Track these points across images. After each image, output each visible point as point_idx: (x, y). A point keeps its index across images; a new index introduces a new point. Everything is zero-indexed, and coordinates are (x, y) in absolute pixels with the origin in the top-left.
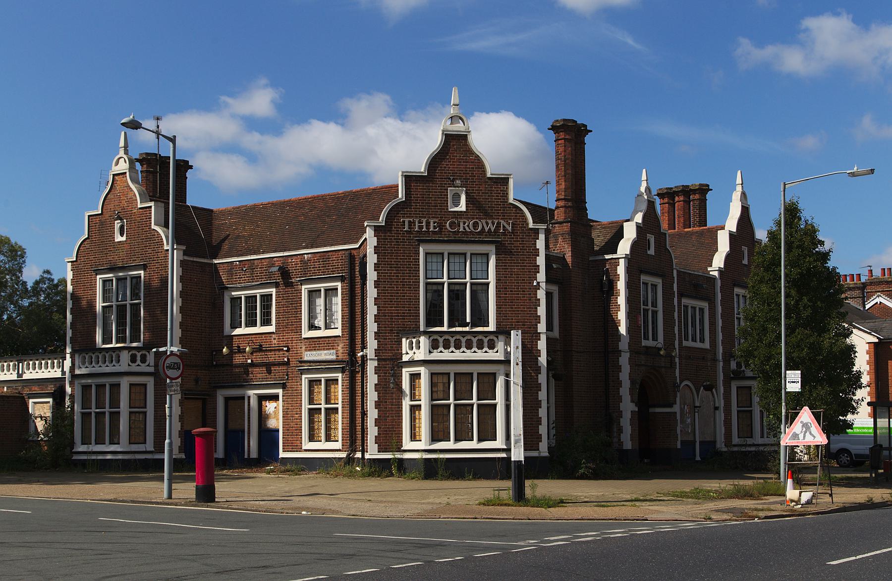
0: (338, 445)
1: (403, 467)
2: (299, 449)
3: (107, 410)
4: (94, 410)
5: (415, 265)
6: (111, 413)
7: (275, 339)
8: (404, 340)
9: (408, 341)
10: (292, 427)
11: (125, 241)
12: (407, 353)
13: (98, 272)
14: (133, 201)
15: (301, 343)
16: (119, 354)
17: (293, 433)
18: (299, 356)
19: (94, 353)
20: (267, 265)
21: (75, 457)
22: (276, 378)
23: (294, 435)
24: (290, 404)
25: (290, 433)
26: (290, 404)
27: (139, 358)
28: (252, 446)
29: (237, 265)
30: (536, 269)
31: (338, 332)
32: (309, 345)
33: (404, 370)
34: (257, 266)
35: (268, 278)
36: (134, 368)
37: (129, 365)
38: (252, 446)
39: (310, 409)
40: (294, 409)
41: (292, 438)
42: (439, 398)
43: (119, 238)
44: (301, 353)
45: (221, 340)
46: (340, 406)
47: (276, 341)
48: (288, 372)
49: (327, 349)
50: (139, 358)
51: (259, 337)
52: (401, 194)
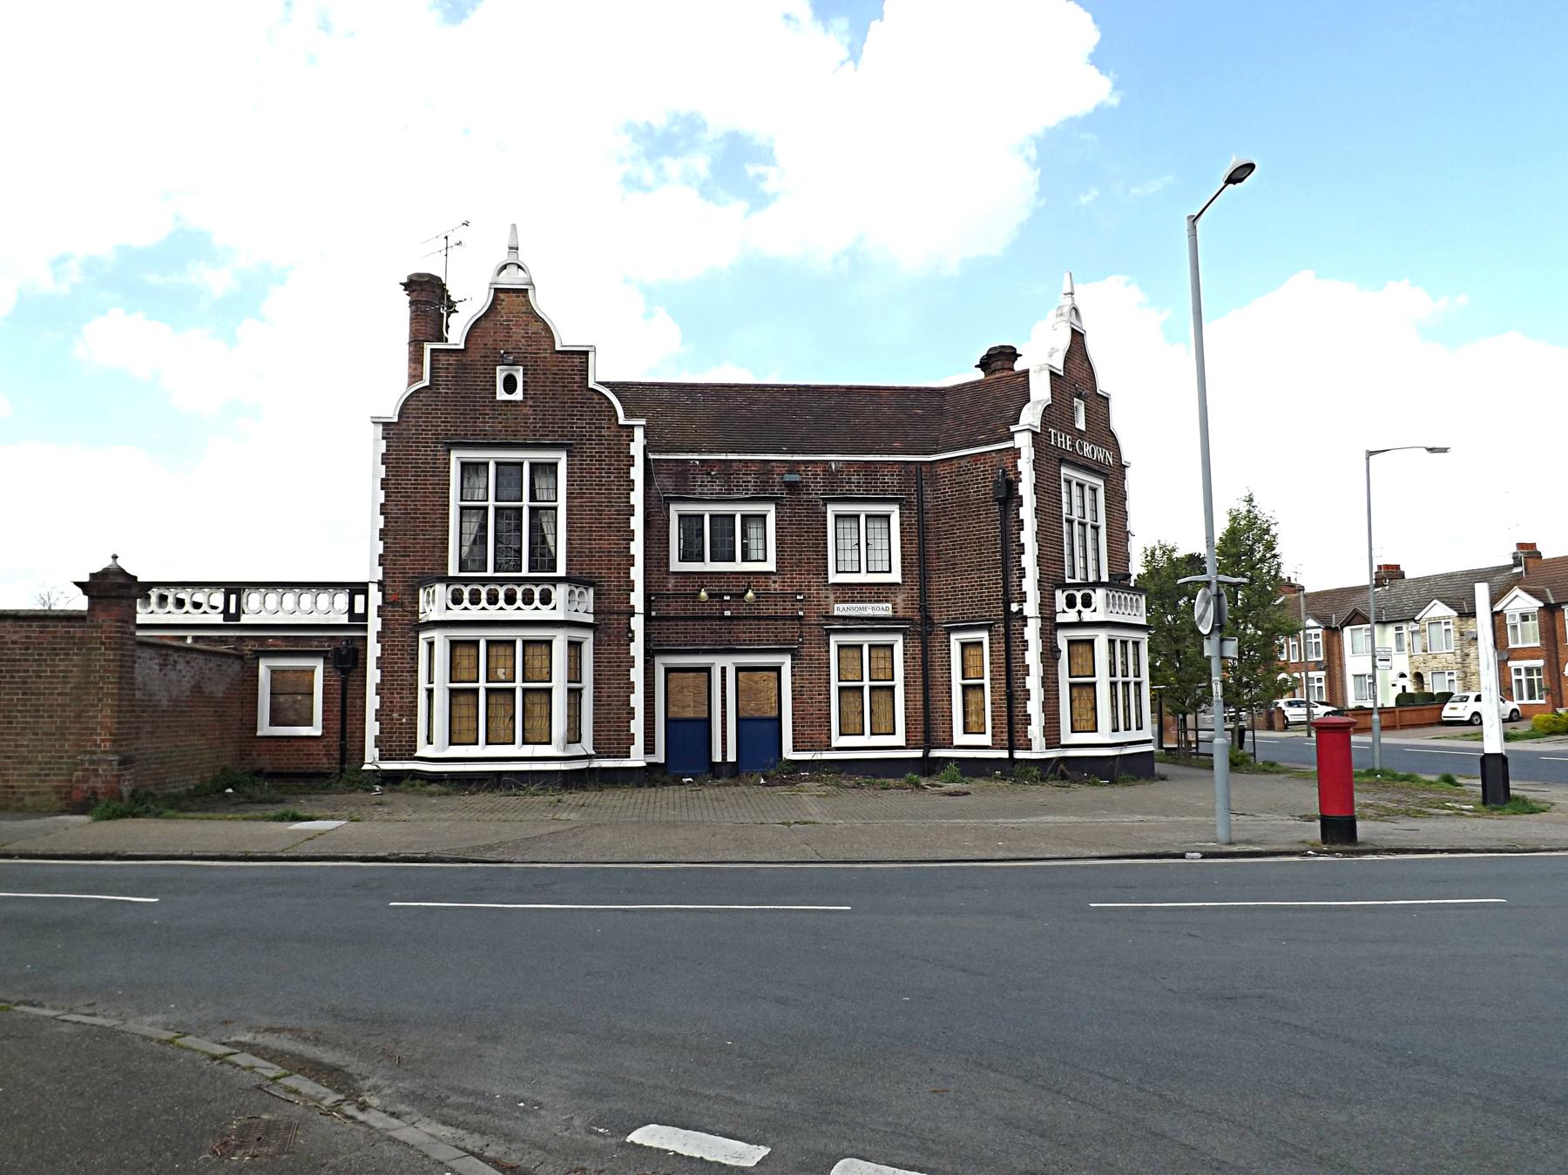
2: (829, 748)
7: (775, 582)
8: (421, 591)
11: (521, 402)
12: (1064, 612)
13: (450, 446)
14: (540, 337)
15: (828, 590)
16: (1090, 596)
19: (577, 587)
21: (732, 757)
22: (779, 640)
26: (807, 679)
27: (1079, 600)
28: (725, 746)
29: (697, 466)
30: (630, 510)
31: (896, 577)
35: (760, 490)
36: (457, 613)
37: (554, 608)
38: (725, 746)
42: (463, 679)
43: (501, 395)
45: (664, 578)
46: (987, 682)
47: (777, 585)
49: (876, 602)
50: (1079, 600)
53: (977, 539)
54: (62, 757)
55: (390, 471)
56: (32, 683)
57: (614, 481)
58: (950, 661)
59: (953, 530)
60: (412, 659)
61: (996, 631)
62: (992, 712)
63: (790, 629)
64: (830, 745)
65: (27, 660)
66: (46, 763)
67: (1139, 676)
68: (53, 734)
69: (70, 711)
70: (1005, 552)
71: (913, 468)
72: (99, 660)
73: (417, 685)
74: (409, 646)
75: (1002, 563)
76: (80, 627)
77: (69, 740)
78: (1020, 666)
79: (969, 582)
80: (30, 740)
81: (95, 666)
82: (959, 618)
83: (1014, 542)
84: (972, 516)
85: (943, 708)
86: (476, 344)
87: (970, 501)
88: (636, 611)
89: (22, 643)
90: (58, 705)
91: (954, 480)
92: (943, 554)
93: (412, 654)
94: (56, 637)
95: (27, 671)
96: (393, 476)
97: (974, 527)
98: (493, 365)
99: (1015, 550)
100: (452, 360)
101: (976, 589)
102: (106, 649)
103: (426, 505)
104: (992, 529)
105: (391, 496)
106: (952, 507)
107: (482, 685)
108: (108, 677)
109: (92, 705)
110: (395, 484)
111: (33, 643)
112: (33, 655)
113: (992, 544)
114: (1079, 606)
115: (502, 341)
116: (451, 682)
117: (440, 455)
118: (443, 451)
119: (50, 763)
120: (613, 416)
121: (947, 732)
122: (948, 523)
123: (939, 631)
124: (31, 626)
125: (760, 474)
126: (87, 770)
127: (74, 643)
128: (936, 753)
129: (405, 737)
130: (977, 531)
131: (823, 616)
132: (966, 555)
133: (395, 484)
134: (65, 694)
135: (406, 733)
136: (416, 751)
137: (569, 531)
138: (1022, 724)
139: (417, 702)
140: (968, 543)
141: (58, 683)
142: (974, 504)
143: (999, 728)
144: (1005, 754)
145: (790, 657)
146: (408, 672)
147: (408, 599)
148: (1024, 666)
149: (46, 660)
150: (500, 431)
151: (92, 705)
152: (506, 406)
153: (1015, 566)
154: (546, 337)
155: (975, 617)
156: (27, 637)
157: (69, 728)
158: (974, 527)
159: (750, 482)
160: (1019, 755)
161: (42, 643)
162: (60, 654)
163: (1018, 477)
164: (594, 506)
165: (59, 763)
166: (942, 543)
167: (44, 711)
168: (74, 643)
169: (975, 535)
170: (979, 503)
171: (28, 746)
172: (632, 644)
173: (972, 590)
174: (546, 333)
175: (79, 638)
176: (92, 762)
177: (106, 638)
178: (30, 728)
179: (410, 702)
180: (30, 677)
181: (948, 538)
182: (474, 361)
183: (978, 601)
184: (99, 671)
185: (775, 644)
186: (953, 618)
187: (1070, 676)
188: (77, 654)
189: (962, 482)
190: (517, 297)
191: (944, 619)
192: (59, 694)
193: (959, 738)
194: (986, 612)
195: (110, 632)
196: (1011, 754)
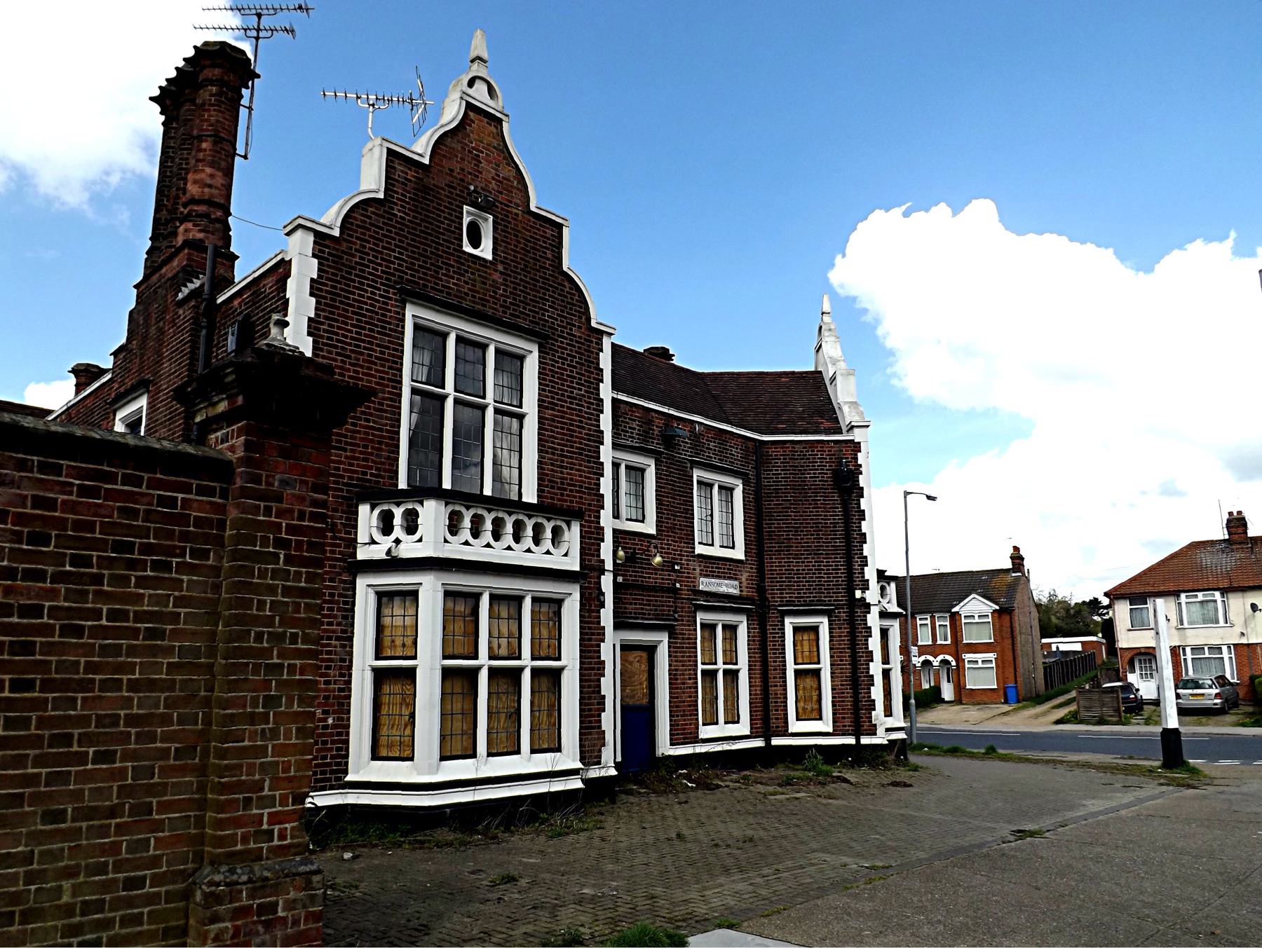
0: (743, 728)
1: (796, 755)
2: (695, 740)
3: (720, 666)
4: (720, 666)
5: (394, 356)
6: (726, 672)
8: (364, 509)
9: (376, 512)
10: (684, 702)
11: (490, 261)
12: (373, 542)
17: (684, 711)
18: (692, 582)
20: (641, 418)
23: (687, 715)
24: (681, 661)
25: (680, 711)
26: (681, 661)
31: (739, 553)
32: (705, 567)
33: (362, 583)
34: (624, 413)
36: (455, 550)
39: (375, 670)
40: (686, 670)
41: (685, 720)
44: (694, 578)
48: (676, 607)
51: (630, 539)
52: (468, 248)
53: (814, 523)
54: (138, 883)
55: (323, 310)
56: (49, 648)
57: (584, 396)
58: (784, 645)
59: (787, 512)
60: (345, 617)
61: (836, 617)
62: (833, 697)
63: (668, 600)
64: (698, 737)
65: (40, 576)
66: (87, 908)
67: (888, 663)
68: (113, 812)
69: (167, 738)
70: (848, 538)
71: (750, 444)
72: (272, 590)
73: (351, 661)
74: (340, 595)
75: (764, 551)
76: (201, 491)
77: (158, 826)
78: (863, 652)
79: (805, 566)
80: (36, 837)
81: (261, 604)
82: (794, 601)
83: (855, 531)
84: (808, 500)
85: (777, 694)
86: (439, 165)
87: (807, 485)
88: (606, 568)
89: (20, 519)
90: (132, 720)
91: (788, 463)
92: (775, 535)
93: (346, 610)
94: (133, 514)
95: (37, 611)
96: (326, 318)
97: (811, 512)
98: (460, 202)
99: (856, 538)
100: (411, 174)
101: (814, 574)
102: (289, 560)
103: (372, 376)
104: (831, 516)
105: (322, 350)
106: (785, 489)
107: (526, 661)
108: (294, 638)
109: (252, 719)
110: (327, 332)
111: (61, 523)
112: (58, 559)
113: (831, 531)
114: (398, 532)
115: (470, 173)
116: (377, 658)
117: (393, 306)
118: (396, 300)
119: (99, 906)
120: (583, 313)
121: (781, 719)
122: (782, 504)
123: (773, 615)
124: (57, 470)
125: (643, 422)
126: (245, 911)
127: (185, 536)
128: (776, 741)
129: (331, 749)
130: (814, 515)
131: (691, 590)
132: (802, 539)
133: (327, 332)
134: (152, 685)
135: (333, 742)
136: (347, 774)
137: (541, 450)
138: (866, 709)
139: (350, 690)
140: (804, 527)
141: (132, 651)
142: (810, 489)
143: (840, 714)
144: (851, 741)
145: (666, 635)
146: (338, 639)
147: (341, 518)
148: (867, 652)
149: (98, 579)
150: (467, 294)
151: (252, 719)
152: (473, 262)
153: (857, 554)
154: (518, 189)
155: (813, 601)
156: (38, 502)
157: (162, 788)
158: (811, 512)
159: (634, 429)
160: (865, 740)
161: (90, 527)
162: (142, 565)
163: (858, 469)
164: (566, 424)
165: (130, 902)
166: (774, 524)
167: (85, 739)
168: (185, 536)
169: (812, 519)
170: (816, 489)
171: (27, 859)
172: (602, 610)
173: (809, 574)
174: (518, 183)
175: (199, 522)
176: (259, 887)
177: (291, 529)
178: (36, 799)
179: (340, 690)
180: (46, 630)
181: (782, 520)
182: (437, 187)
183: (816, 585)
184: (269, 622)
185: (656, 619)
186: (787, 601)
187: (796, 664)
188: (191, 569)
189: (797, 466)
190: (488, 123)
191: (777, 602)
192: (134, 686)
193: (795, 726)
194: (825, 597)
195: (302, 516)
196: (858, 740)
